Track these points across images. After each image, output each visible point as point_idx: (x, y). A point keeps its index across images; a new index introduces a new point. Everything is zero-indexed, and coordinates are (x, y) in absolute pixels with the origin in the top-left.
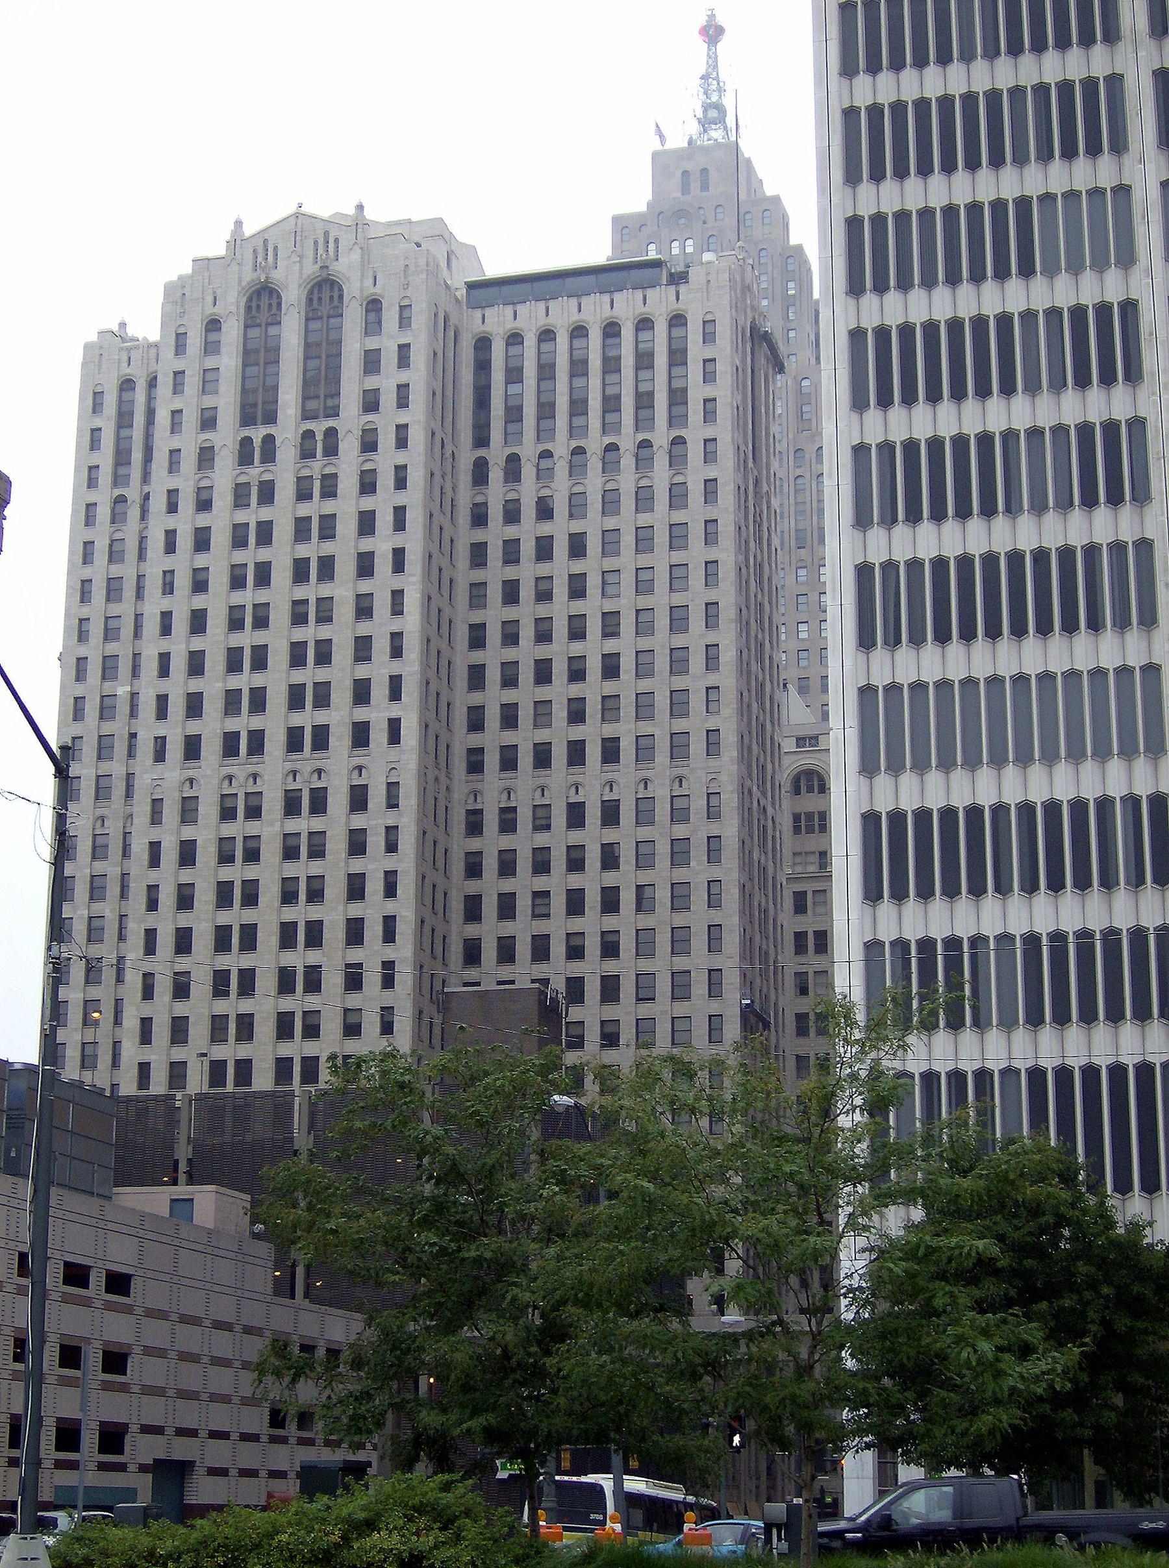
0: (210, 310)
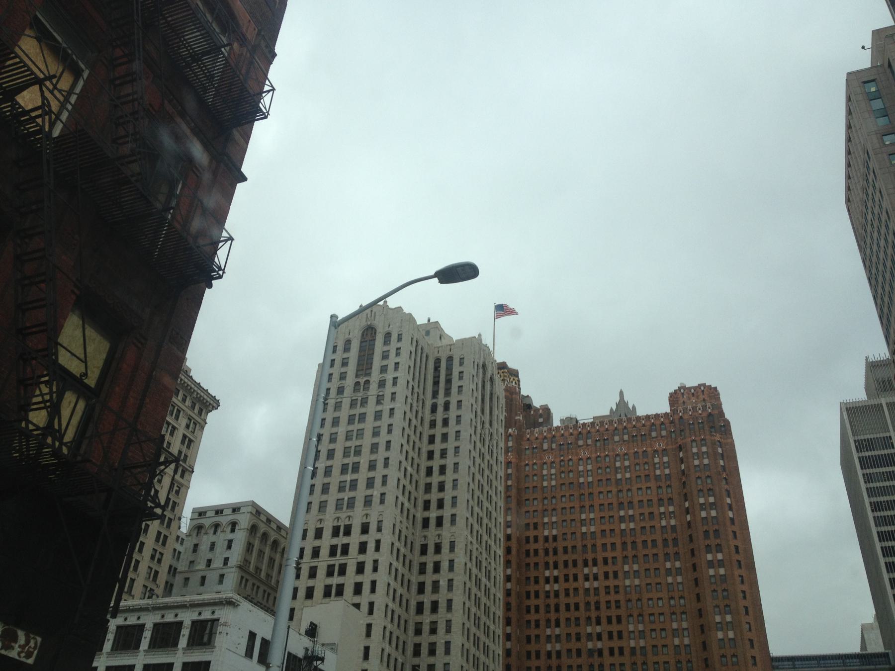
0: (347, 336)
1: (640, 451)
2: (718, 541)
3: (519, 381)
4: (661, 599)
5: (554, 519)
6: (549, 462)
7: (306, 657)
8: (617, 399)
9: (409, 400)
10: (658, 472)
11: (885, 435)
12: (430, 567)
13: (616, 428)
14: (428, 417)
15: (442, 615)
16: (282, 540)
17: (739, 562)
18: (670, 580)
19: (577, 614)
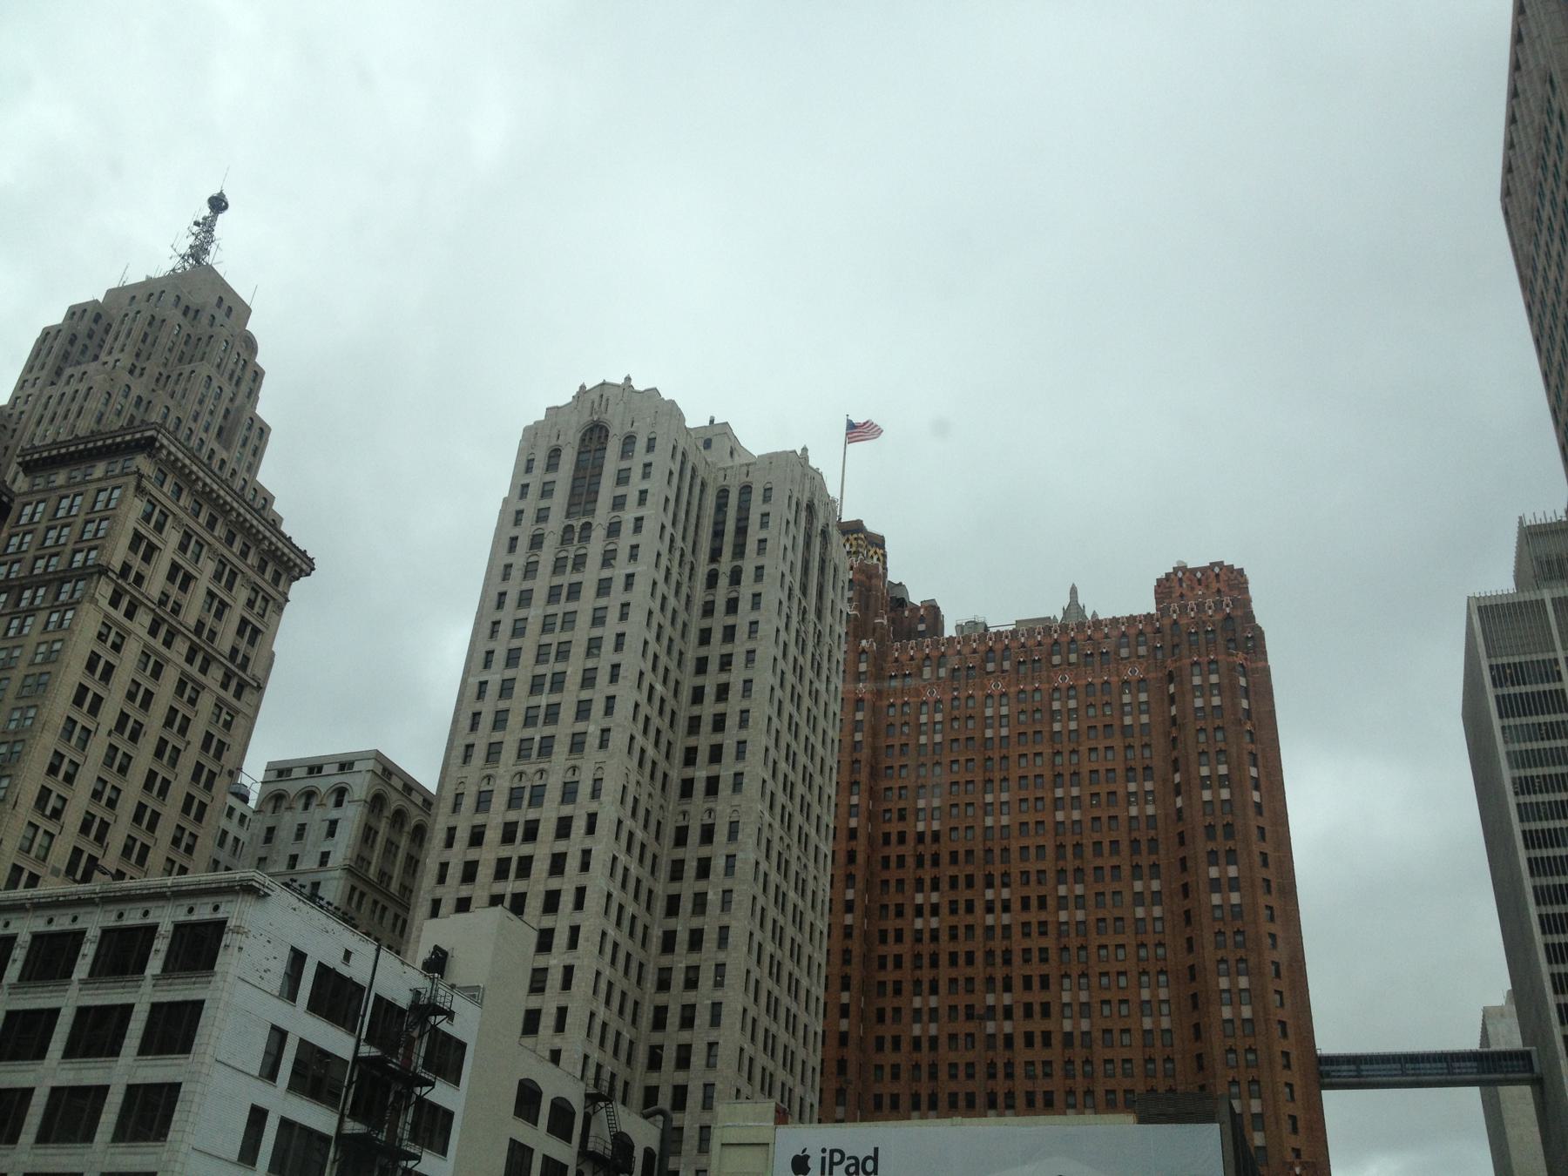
0: (554, 442)
1: (1097, 681)
2: (1230, 844)
3: (884, 556)
4: (1122, 946)
6: (932, 700)
7: (415, 1006)
8: (1066, 602)
9: (664, 561)
10: (1128, 721)
11: (1546, 656)
12: (691, 868)
13: (1056, 642)
17: (1267, 881)
18: (1140, 912)
19: (969, 971)
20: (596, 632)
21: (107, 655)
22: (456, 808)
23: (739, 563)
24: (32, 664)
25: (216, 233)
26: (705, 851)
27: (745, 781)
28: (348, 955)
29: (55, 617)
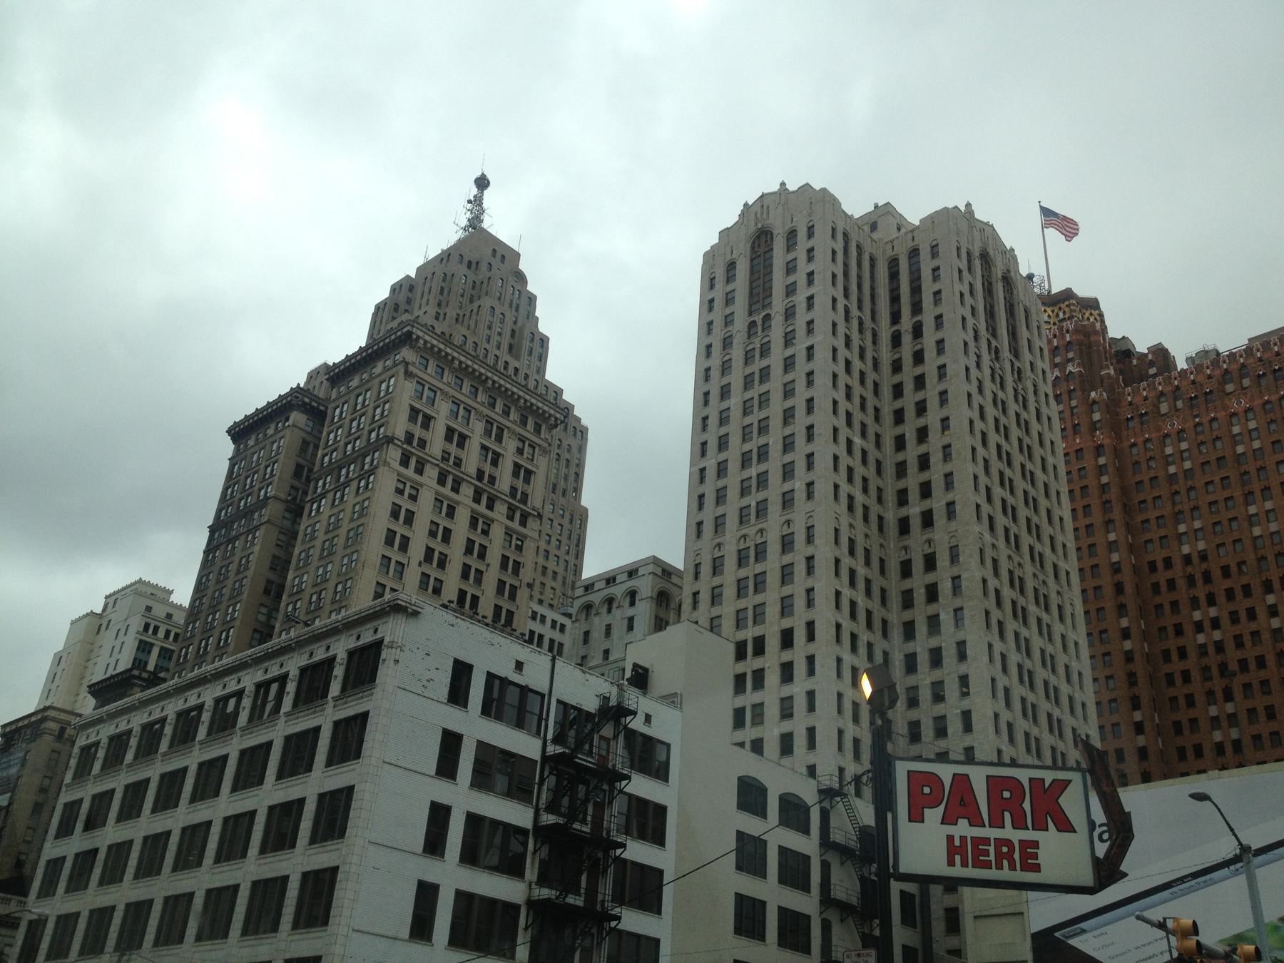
0: (729, 257)
3: (1101, 315)
5: (1197, 524)
9: (841, 329)
14: (886, 356)
15: (950, 670)
16: (674, 591)
20: (789, 403)
21: (406, 504)
22: (697, 576)
23: (919, 318)
24: (352, 520)
25: (485, 206)
26: (930, 578)
27: (958, 508)
28: (519, 666)
29: (363, 483)
